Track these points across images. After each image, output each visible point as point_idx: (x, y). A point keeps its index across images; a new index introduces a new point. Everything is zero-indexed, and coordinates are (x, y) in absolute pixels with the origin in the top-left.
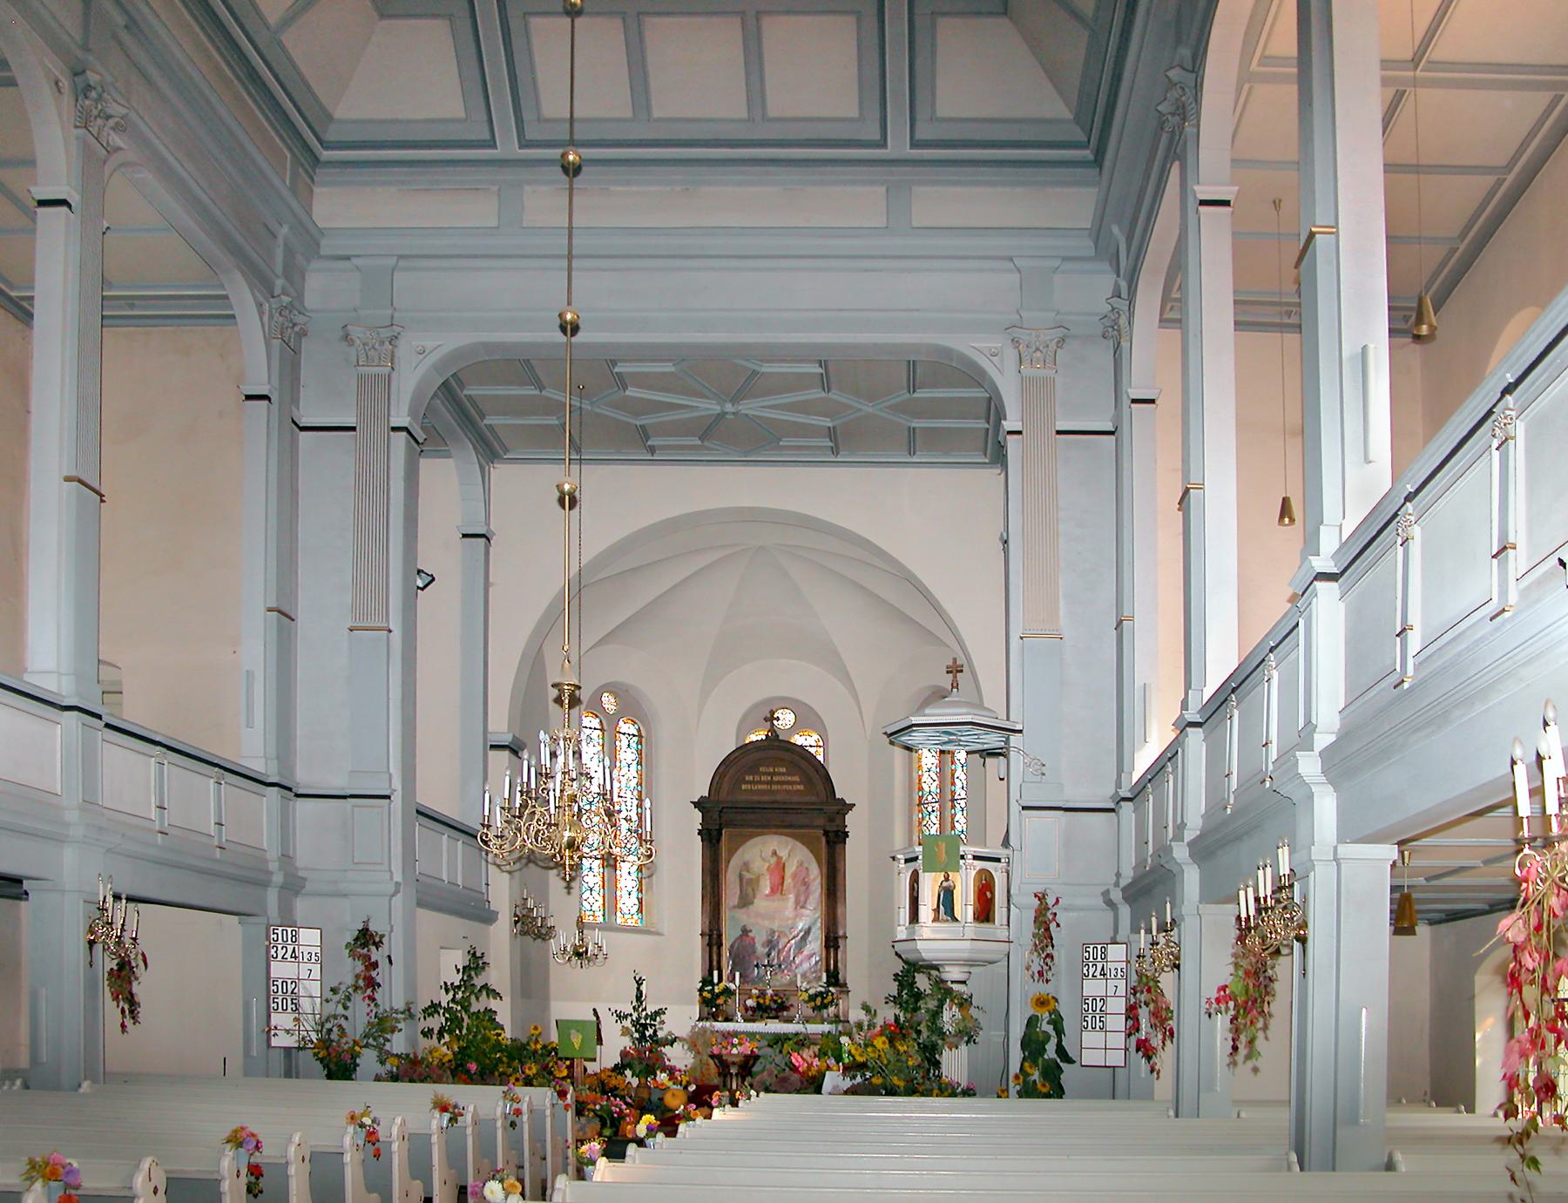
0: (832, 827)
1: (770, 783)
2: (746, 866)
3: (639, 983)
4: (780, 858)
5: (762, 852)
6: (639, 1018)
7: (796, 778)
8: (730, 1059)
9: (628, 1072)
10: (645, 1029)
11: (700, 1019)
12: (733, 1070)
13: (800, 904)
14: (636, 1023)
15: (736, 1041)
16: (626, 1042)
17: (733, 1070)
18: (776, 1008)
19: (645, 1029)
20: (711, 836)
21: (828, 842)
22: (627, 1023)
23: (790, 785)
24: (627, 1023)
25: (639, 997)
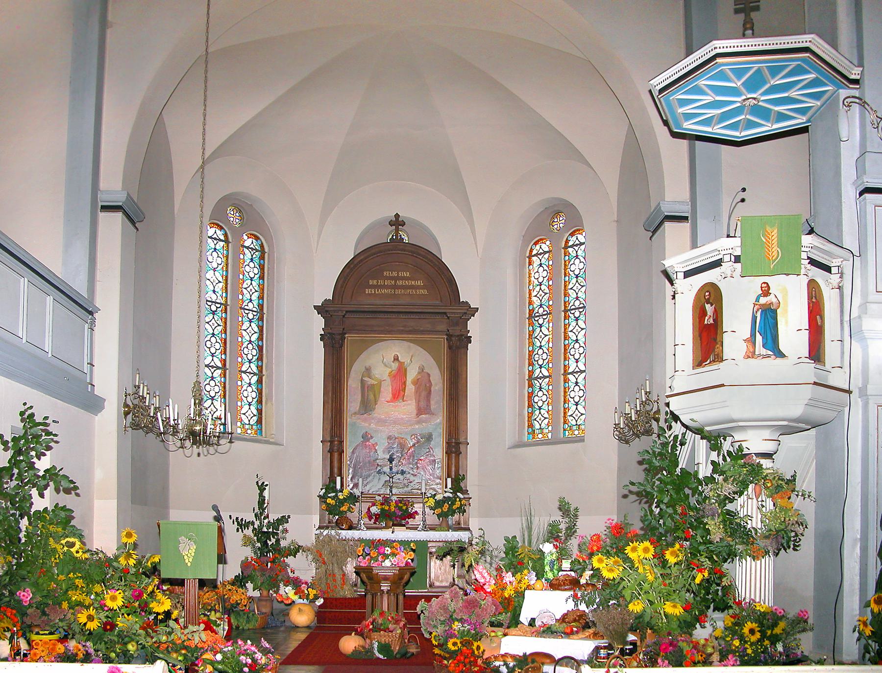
0: (456, 331)
1: (395, 287)
2: (368, 371)
3: (262, 488)
4: (401, 364)
5: (386, 359)
6: (261, 526)
7: (420, 283)
8: (382, 573)
9: (250, 585)
10: (268, 542)
11: (320, 528)
12: (385, 587)
13: (423, 410)
14: (258, 532)
15: (388, 550)
16: (248, 553)
17: (385, 587)
18: (396, 514)
19: (268, 542)
20: (333, 342)
21: (450, 347)
22: (249, 532)
23: (415, 289)
24: (249, 532)
25: (261, 501)
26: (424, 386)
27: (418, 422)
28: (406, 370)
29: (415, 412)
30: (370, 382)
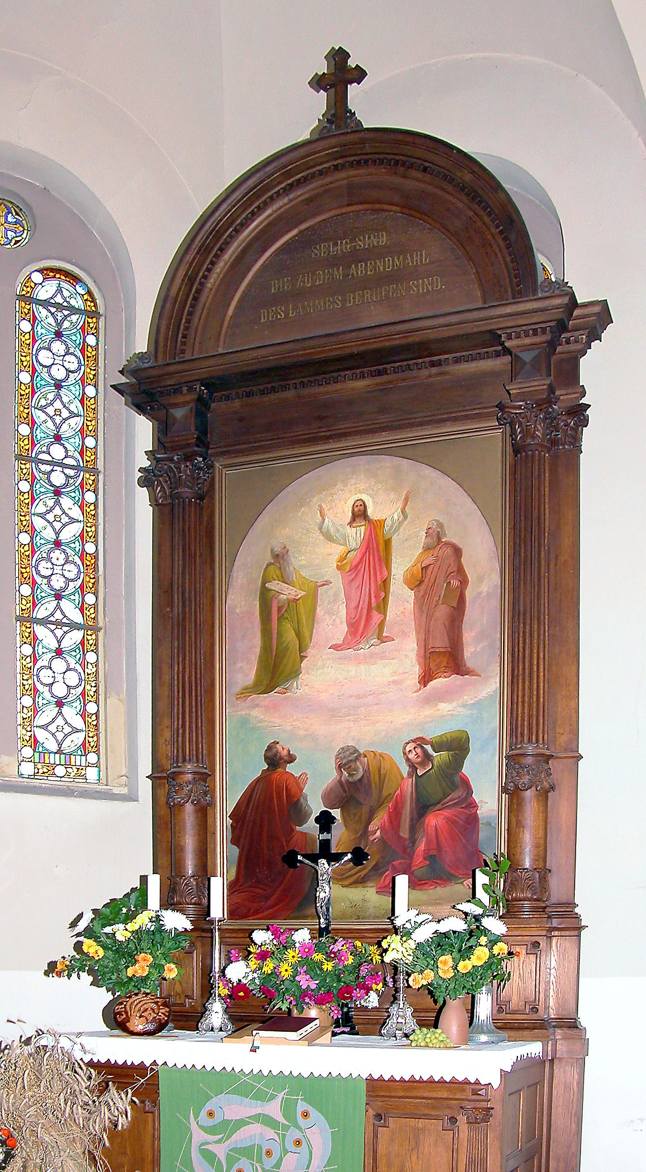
2: (279, 558)
4: (375, 527)
5: (334, 514)
13: (444, 658)
26: (442, 583)
27: (430, 700)
28: (388, 543)
29: (416, 671)
30: (286, 592)
